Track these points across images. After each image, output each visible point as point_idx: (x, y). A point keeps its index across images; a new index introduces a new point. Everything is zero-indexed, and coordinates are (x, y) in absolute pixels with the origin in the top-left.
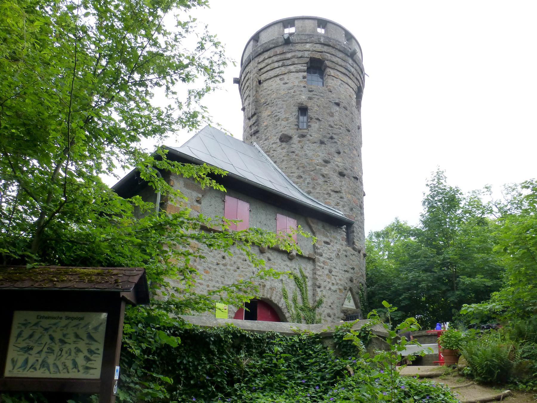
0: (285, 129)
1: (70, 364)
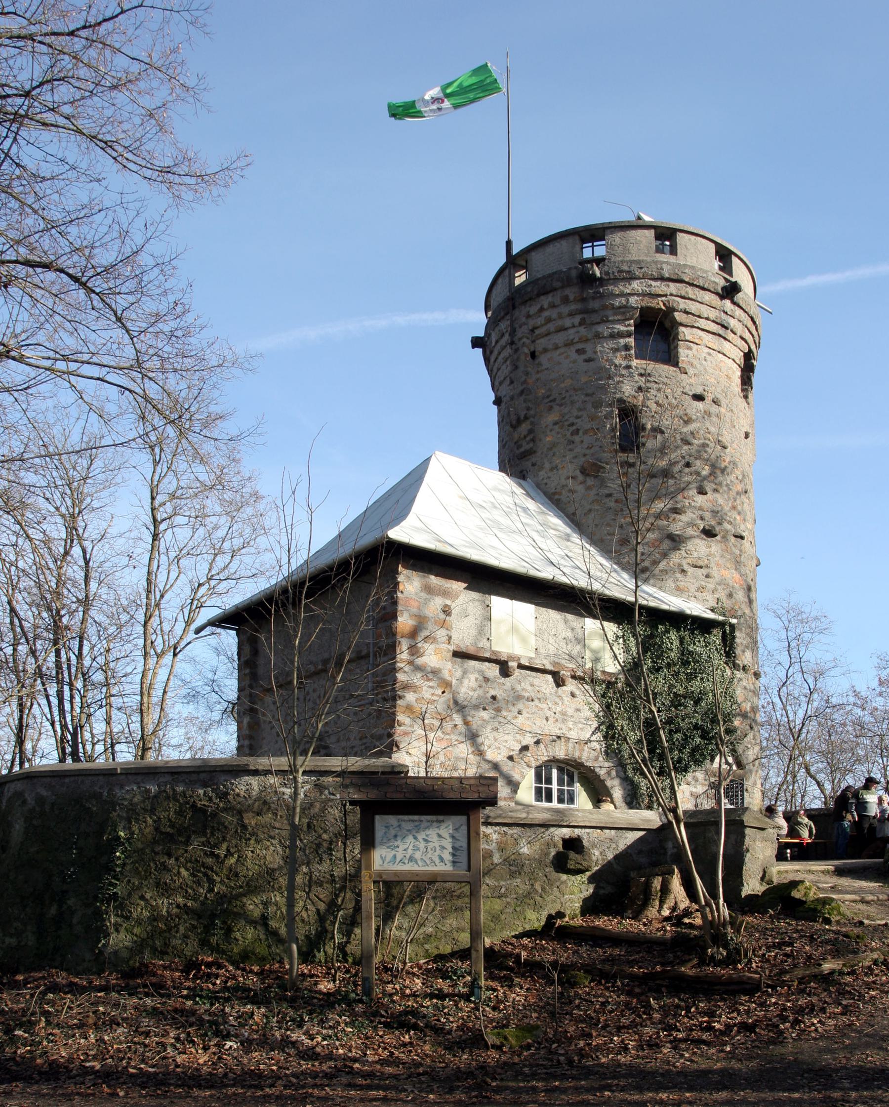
0: (592, 451)
1: (437, 861)
